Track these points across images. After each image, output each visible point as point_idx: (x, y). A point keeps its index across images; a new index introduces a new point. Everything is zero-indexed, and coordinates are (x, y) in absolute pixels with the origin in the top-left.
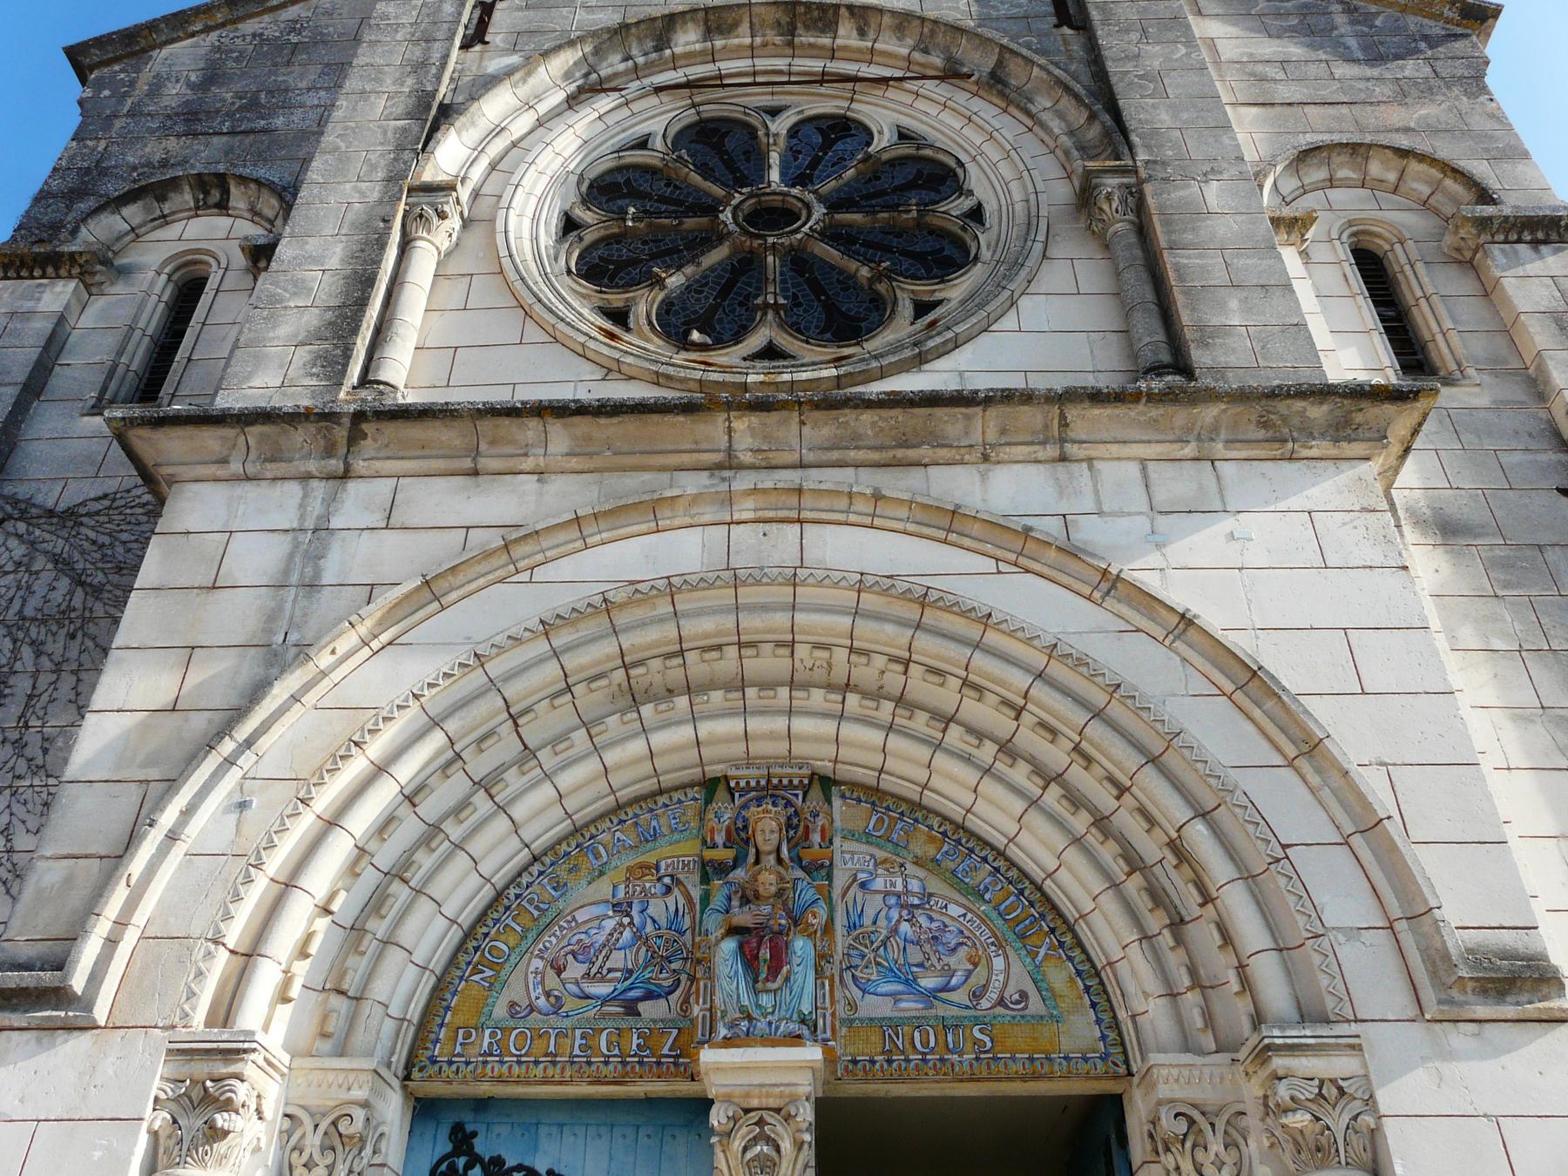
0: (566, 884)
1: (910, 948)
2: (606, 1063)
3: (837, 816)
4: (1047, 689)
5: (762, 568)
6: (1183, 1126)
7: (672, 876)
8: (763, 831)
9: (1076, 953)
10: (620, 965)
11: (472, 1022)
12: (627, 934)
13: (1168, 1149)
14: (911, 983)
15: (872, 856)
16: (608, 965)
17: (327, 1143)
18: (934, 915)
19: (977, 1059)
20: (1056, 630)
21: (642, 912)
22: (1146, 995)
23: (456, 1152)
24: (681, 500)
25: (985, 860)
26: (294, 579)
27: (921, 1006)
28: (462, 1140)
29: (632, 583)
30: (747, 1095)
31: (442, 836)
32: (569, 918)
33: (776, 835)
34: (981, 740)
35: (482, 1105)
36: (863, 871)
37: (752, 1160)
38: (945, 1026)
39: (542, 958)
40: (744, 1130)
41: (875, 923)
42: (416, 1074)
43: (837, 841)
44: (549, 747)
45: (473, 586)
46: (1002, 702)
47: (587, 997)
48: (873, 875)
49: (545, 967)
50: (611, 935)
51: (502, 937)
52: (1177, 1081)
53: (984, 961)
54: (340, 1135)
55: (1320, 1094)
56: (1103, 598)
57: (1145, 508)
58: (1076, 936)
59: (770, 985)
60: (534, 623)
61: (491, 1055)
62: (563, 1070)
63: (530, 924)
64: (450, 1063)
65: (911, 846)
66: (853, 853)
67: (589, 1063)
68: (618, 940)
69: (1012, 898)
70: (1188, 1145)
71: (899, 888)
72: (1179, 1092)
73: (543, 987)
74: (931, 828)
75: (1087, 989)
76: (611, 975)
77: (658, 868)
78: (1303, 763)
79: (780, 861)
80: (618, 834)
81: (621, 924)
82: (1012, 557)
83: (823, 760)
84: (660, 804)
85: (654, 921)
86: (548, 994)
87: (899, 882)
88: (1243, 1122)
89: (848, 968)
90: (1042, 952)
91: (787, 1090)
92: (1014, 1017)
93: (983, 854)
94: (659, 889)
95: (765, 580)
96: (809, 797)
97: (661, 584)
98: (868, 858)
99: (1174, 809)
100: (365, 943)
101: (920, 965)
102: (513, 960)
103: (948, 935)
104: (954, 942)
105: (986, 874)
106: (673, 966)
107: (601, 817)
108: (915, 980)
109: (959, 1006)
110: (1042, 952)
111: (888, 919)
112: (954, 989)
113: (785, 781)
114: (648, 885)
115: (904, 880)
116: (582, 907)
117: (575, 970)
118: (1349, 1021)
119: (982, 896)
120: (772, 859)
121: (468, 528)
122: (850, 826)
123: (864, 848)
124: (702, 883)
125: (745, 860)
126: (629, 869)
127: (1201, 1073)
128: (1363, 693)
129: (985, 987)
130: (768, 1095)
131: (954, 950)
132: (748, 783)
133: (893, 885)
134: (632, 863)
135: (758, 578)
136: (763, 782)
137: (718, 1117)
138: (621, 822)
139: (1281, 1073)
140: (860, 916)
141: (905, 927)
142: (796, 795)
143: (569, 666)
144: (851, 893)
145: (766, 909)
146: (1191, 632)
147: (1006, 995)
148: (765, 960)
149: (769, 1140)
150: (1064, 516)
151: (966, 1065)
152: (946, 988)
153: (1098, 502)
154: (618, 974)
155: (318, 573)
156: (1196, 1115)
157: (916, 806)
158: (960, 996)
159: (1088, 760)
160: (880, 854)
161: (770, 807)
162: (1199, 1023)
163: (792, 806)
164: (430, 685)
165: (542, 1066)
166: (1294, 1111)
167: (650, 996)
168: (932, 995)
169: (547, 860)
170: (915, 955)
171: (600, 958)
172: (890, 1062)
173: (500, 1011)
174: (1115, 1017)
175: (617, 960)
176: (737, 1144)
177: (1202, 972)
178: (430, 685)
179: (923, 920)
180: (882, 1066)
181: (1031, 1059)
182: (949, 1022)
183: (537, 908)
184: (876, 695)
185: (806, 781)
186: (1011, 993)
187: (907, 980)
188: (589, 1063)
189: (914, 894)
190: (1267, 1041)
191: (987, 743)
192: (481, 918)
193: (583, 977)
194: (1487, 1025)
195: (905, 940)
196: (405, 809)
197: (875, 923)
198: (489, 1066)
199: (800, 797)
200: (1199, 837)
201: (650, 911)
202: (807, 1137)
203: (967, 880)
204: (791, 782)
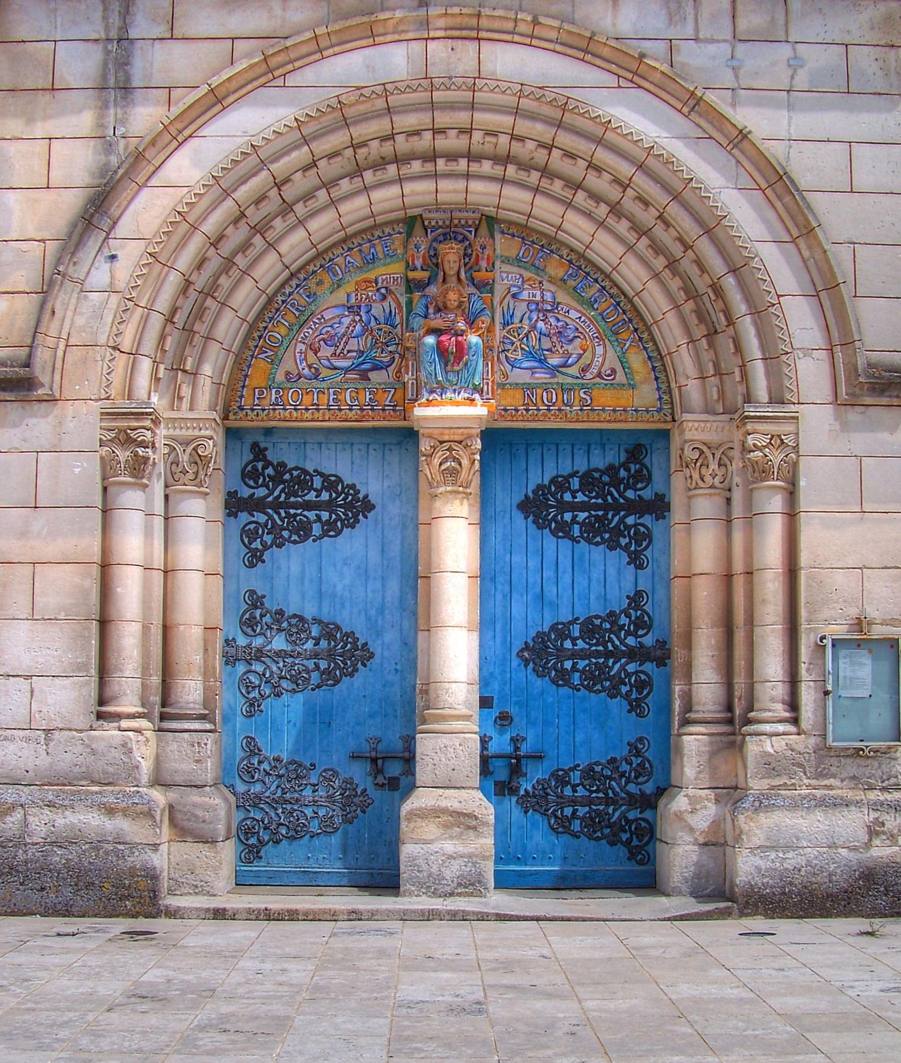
0: (315, 294)
1: (543, 338)
3: (498, 247)
4: (644, 178)
5: (450, 78)
6: (696, 455)
7: (386, 288)
8: (449, 262)
9: (650, 345)
11: (263, 385)
12: (358, 327)
13: (687, 467)
14: (542, 361)
16: (347, 348)
17: (192, 460)
18: (560, 317)
20: (655, 135)
21: (367, 312)
22: (688, 377)
23: (256, 459)
24: (391, 21)
25: (596, 281)
26: (112, 83)
28: (258, 452)
29: (359, 88)
31: (235, 267)
33: (458, 264)
34: (598, 203)
36: (515, 286)
37: (445, 470)
38: (563, 389)
39: (304, 343)
40: (440, 453)
41: (521, 321)
42: (231, 416)
43: (498, 264)
44: (301, 202)
45: (244, 91)
46: (614, 180)
47: (336, 368)
49: (306, 350)
50: (348, 328)
51: (276, 330)
54: (200, 456)
55: (770, 443)
56: (689, 112)
57: (729, 37)
58: (651, 334)
59: (456, 368)
63: (294, 321)
64: (252, 410)
65: (547, 270)
66: (508, 273)
68: (352, 331)
70: (698, 464)
71: (538, 298)
72: (697, 436)
74: (561, 257)
75: (654, 368)
76: (349, 355)
77: (376, 283)
78: (801, 243)
79: (459, 279)
80: (348, 258)
81: (354, 321)
82: (630, 76)
83: (488, 207)
84: (376, 236)
85: (376, 319)
86: (310, 367)
87: (538, 293)
88: (731, 453)
89: (503, 351)
90: (627, 345)
91: (466, 431)
92: (606, 385)
93: (595, 276)
95: (453, 87)
96: (478, 233)
97: (379, 90)
98: (518, 277)
99: (717, 265)
100: (196, 339)
102: (285, 345)
103: (568, 331)
104: (572, 335)
105: (596, 290)
106: (390, 349)
107: (334, 245)
108: (545, 359)
109: (572, 377)
110: (627, 345)
111: (530, 319)
112: (570, 366)
113: (463, 222)
114: (370, 294)
115: (542, 293)
116: (327, 309)
118: (794, 404)
119: (593, 306)
120: (454, 279)
121: (233, 39)
122: (506, 254)
123: (516, 269)
124: (406, 293)
125: (436, 279)
128: (852, 192)
130: (454, 434)
131: (571, 341)
132: (437, 222)
133: (534, 296)
134: (359, 279)
135: (449, 82)
136: (448, 223)
137: (425, 446)
138: (350, 249)
139: (750, 432)
141: (540, 324)
142: (470, 232)
143: (315, 151)
144: (506, 301)
145: (452, 316)
146: (745, 143)
148: (452, 353)
149: (455, 459)
150: (671, 40)
152: (565, 365)
153: (697, 30)
155: (128, 79)
156: (705, 449)
157: (553, 240)
158: (574, 371)
159: (667, 225)
160: (527, 275)
162: (715, 396)
163: (467, 240)
166: (754, 451)
167: (375, 368)
168: (554, 370)
169: (302, 276)
170: (546, 344)
172: (527, 410)
173: (280, 377)
174: (669, 386)
175: (353, 344)
176: (436, 461)
177: (723, 365)
181: (614, 411)
182: (565, 387)
183: (297, 310)
184: (525, 166)
185: (477, 222)
186: (606, 369)
187: (540, 360)
188: (340, 410)
189: (547, 302)
190: (746, 414)
191: (602, 205)
192: (260, 316)
194: (871, 408)
196: (212, 252)
197: (521, 321)
199: (473, 233)
200: (730, 282)
201: (373, 311)
202: (478, 457)
204: (467, 222)
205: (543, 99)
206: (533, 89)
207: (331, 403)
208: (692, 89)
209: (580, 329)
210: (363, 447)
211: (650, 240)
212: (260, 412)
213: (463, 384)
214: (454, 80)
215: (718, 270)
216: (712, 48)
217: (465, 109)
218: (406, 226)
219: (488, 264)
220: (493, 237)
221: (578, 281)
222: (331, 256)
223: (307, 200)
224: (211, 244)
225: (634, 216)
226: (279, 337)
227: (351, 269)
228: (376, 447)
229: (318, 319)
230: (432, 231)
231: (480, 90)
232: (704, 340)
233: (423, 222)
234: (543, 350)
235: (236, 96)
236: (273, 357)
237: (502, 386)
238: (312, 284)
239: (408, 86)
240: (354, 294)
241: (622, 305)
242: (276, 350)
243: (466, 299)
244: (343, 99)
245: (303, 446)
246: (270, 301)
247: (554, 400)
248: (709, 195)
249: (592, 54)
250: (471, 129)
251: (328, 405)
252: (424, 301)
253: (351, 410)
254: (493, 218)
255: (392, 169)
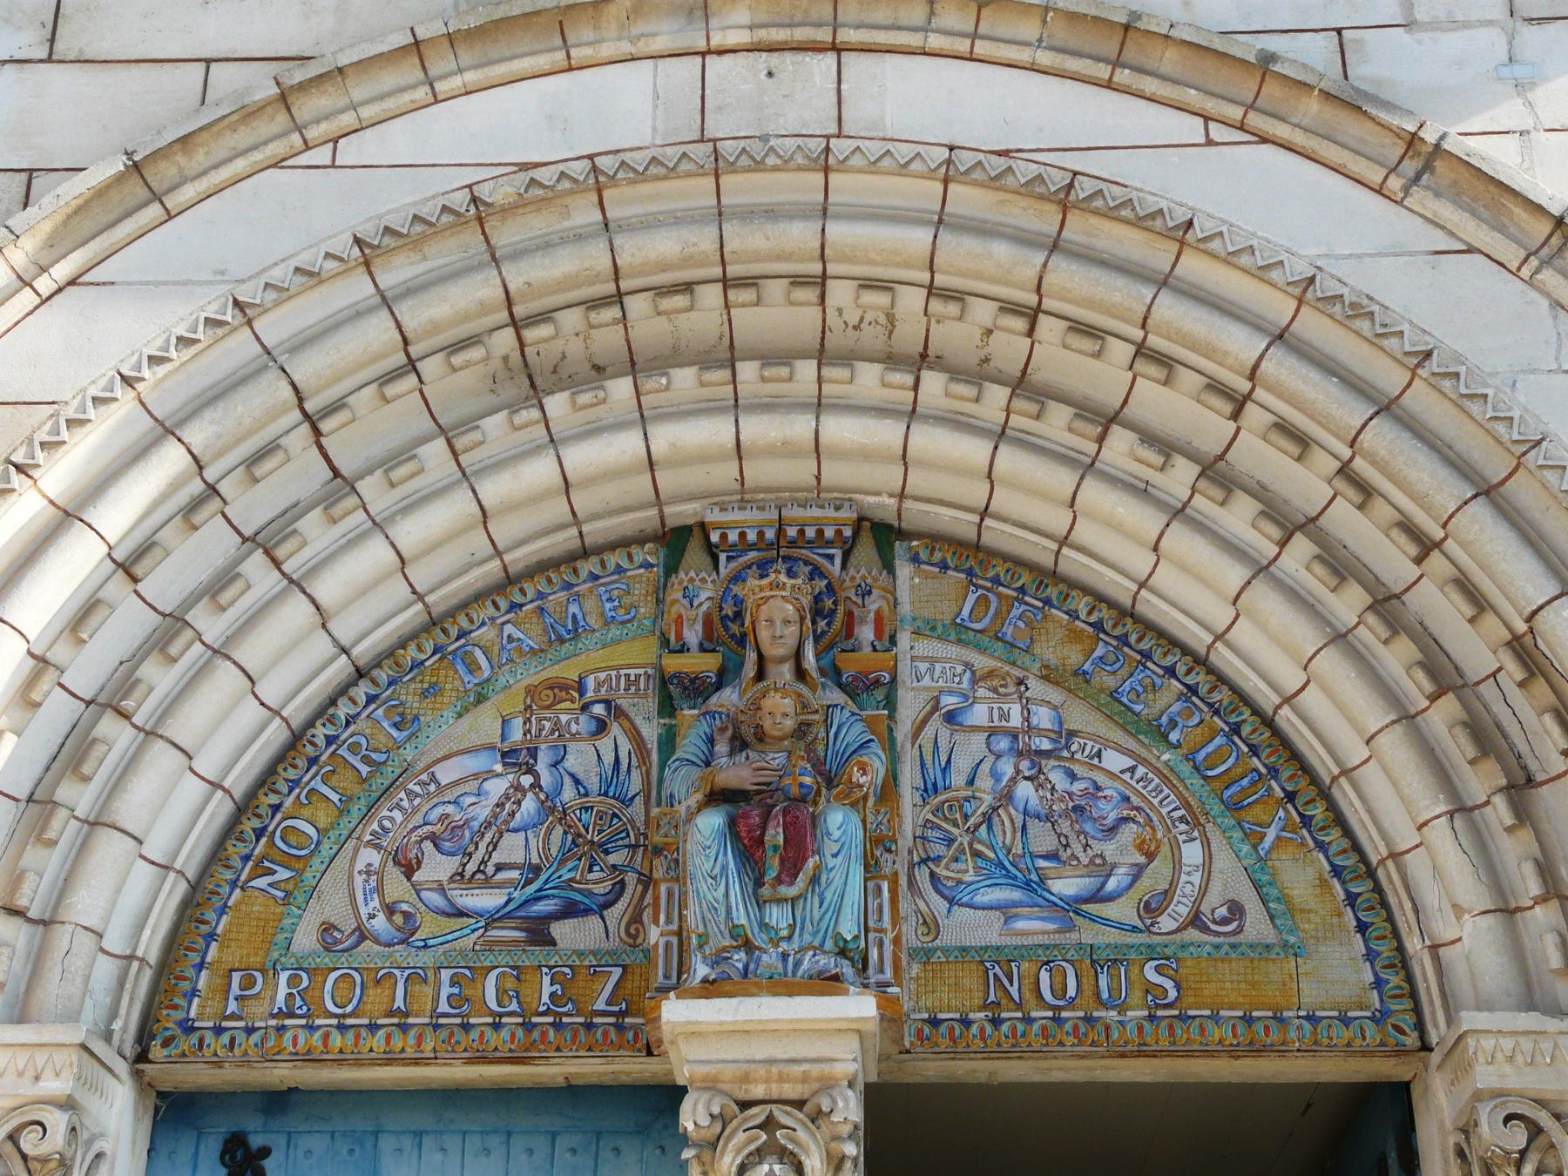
0: (416, 718)
1: (1034, 827)
2: (497, 1026)
4: (1292, 361)
5: (764, 138)
6: (1517, 1138)
7: (607, 703)
8: (770, 621)
10: (519, 858)
11: (255, 960)
12: (529, 804)
14: (1034, 886)
15: (968, 665)
16: (497, 857)
18: (1077, 769)
19: (1151, 1018)
21: (555, 765)
25: (1171, 672)
27: (1052, 926)
29: (524, 167)
30: (746, 1079)
32: (424, 777)
35: (277, 1101)
36: (951, 692)
38: (1095, 961)
39: (378, 847)
40: (741, 1137)
41: (971, 782)
42: (157, 1051)
43: (904, 639)
45: (224, 174)
47: (460, 913)
48: (970, 700)
49: (383, 863)
50: (500, 805)
51: (305, 812)
52: (1511, 1059)
53: (1165, 849)
54: (24, 1157)
56: (1406, 190)
59: (792, 891)
60: (342, 244)
61: (291, 1015)
62: (420, 1039)
64: (219, 1031)
65: (1037, 650)
66: (932, 660)
67: (466, 1027)
69: (1219, 741)
71: (1016, 721)
72: (1513, 1079)
73: (382, 896)
74: (1073, 615)
75: (1351, 899)
76: (502, 876)
77: (581, 687)
79: (801, 674)
80: (509, 629)
81: (518, 787)
82: (1235, 113)
83: (878, 494)
85: (577, 782)
86: (390, 910)
89: (924, 861)
90: (1271, 834)
91: (815, 1069)
92: (1217, 947)
94: (584, 725)
95: (771, 160)
96: (853, 560)
97: (579, 169)
98: (959, 669)
100: (56, 824)
101: (1052, 856)
102: (326, 849)
103: (1101, 804)
104: (1113, 816)
106: (613, 859)
107: (478, 597)
109: (1120, 926)
110: (1271, 834)
111: (995, 775)
112: (1111, 898)
113: (810, 533)
114: (564, 718)
117: (437, 867)
119: (1165, 737)
120: (786, 671)
122: (928, 612)
123: (952, 651)
124: (661, 714)
126: (530, 691)
127: (1556, 1046)
129: (1167, 895)
130: (781, 1079)
131: (1112, 830)
132: (743, 535)
133: (1005, 716)
134: (535, 680)
136: (770, 534)
137: (693, 1116)
138: (514, 607)
140: (944, 771)
141: (1025, 790)
142: (831, 558)
144: (928, 731)
145: (777, 759)
147: (1205, 908)
148: (776, 848)
150: (1339, 31)
151: (1131, 1030)
152: (1097, 897)
154: (514, 874)
156: (1544, 1118)
158: (1123, 910)
159: (1366, 492)
160: (982, 662)
161: (783, 578)
163: (822, 576)
164: (154, 360)
165: (381, 1033)
167: (571, 910)
168: (1074, 907)
169: (382, 676)
171: (482, 846)
172: (996, 1022)
173: (306, 939)
174: (1400, 949)
175: (513, 849)
178: (154, 360)
179: (1057, 778)
180: (982, 1030)
181: (1248, 1020)
183: (366, 760)
185: (848, 532)
186: (1214, 904)
187: (1028, 883)
189: (1041, 732)
191: (1180, 462)
192: (266, 779)
193: (451, 880)
195: (1026, 812)
196: (118, 587)
197: (971, 782)
198: (289, 1035)
199: (838, 561)
201: (571, 763)
202: (851, 1149)
203: (1138, 708)
204: (820, 533)
205: (1009, 181)
206: (981, 156)
207: (444, 1007)
208: (1412, 128)
209: (1135, 800)
210: (541, 1144)
211: (1317, 543)
212: (241, 1037)
213: (807, 938)
214: (772, 142)
215: (1530, 590)
216: (1452, 42)
217: (805, 216)
218: (662, 552)
219: (879, 632)
220: (889, 568)
221: (1123, 673)
222: (464, 623)
223: (391, 468)
224: (119, 565)
225: (1264, 487)
226: (311, 831)
227: (515, 656)
228: (575, 1140)
229: (423, 784)
230: (729, 559)
231: (843, 166)
232: (1500, 802)
233: (707, 537)
234: (1033, 856)
235: (203, 185)
236: (290, 887)
237: (924, 955)
238: (409, 695)
239: (654, 158)
240: (520, 720)
241: (1246, 730)
242: (298, 866)
243: (816, 717)
244: (484, 192)
245: (369, 1144)
246: (297, 739)
247: (1071, 992)
248: (1485, 391)
249: (1132, 68)
250: (824, 276)
251: (435, 1014)
252: (704, 727)
253: (497, 1026)
254: (889, 527)
255: (621, 388)
